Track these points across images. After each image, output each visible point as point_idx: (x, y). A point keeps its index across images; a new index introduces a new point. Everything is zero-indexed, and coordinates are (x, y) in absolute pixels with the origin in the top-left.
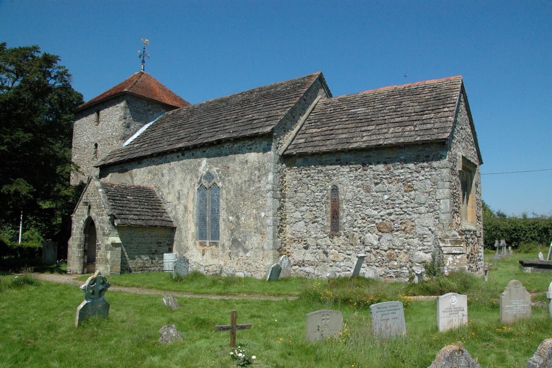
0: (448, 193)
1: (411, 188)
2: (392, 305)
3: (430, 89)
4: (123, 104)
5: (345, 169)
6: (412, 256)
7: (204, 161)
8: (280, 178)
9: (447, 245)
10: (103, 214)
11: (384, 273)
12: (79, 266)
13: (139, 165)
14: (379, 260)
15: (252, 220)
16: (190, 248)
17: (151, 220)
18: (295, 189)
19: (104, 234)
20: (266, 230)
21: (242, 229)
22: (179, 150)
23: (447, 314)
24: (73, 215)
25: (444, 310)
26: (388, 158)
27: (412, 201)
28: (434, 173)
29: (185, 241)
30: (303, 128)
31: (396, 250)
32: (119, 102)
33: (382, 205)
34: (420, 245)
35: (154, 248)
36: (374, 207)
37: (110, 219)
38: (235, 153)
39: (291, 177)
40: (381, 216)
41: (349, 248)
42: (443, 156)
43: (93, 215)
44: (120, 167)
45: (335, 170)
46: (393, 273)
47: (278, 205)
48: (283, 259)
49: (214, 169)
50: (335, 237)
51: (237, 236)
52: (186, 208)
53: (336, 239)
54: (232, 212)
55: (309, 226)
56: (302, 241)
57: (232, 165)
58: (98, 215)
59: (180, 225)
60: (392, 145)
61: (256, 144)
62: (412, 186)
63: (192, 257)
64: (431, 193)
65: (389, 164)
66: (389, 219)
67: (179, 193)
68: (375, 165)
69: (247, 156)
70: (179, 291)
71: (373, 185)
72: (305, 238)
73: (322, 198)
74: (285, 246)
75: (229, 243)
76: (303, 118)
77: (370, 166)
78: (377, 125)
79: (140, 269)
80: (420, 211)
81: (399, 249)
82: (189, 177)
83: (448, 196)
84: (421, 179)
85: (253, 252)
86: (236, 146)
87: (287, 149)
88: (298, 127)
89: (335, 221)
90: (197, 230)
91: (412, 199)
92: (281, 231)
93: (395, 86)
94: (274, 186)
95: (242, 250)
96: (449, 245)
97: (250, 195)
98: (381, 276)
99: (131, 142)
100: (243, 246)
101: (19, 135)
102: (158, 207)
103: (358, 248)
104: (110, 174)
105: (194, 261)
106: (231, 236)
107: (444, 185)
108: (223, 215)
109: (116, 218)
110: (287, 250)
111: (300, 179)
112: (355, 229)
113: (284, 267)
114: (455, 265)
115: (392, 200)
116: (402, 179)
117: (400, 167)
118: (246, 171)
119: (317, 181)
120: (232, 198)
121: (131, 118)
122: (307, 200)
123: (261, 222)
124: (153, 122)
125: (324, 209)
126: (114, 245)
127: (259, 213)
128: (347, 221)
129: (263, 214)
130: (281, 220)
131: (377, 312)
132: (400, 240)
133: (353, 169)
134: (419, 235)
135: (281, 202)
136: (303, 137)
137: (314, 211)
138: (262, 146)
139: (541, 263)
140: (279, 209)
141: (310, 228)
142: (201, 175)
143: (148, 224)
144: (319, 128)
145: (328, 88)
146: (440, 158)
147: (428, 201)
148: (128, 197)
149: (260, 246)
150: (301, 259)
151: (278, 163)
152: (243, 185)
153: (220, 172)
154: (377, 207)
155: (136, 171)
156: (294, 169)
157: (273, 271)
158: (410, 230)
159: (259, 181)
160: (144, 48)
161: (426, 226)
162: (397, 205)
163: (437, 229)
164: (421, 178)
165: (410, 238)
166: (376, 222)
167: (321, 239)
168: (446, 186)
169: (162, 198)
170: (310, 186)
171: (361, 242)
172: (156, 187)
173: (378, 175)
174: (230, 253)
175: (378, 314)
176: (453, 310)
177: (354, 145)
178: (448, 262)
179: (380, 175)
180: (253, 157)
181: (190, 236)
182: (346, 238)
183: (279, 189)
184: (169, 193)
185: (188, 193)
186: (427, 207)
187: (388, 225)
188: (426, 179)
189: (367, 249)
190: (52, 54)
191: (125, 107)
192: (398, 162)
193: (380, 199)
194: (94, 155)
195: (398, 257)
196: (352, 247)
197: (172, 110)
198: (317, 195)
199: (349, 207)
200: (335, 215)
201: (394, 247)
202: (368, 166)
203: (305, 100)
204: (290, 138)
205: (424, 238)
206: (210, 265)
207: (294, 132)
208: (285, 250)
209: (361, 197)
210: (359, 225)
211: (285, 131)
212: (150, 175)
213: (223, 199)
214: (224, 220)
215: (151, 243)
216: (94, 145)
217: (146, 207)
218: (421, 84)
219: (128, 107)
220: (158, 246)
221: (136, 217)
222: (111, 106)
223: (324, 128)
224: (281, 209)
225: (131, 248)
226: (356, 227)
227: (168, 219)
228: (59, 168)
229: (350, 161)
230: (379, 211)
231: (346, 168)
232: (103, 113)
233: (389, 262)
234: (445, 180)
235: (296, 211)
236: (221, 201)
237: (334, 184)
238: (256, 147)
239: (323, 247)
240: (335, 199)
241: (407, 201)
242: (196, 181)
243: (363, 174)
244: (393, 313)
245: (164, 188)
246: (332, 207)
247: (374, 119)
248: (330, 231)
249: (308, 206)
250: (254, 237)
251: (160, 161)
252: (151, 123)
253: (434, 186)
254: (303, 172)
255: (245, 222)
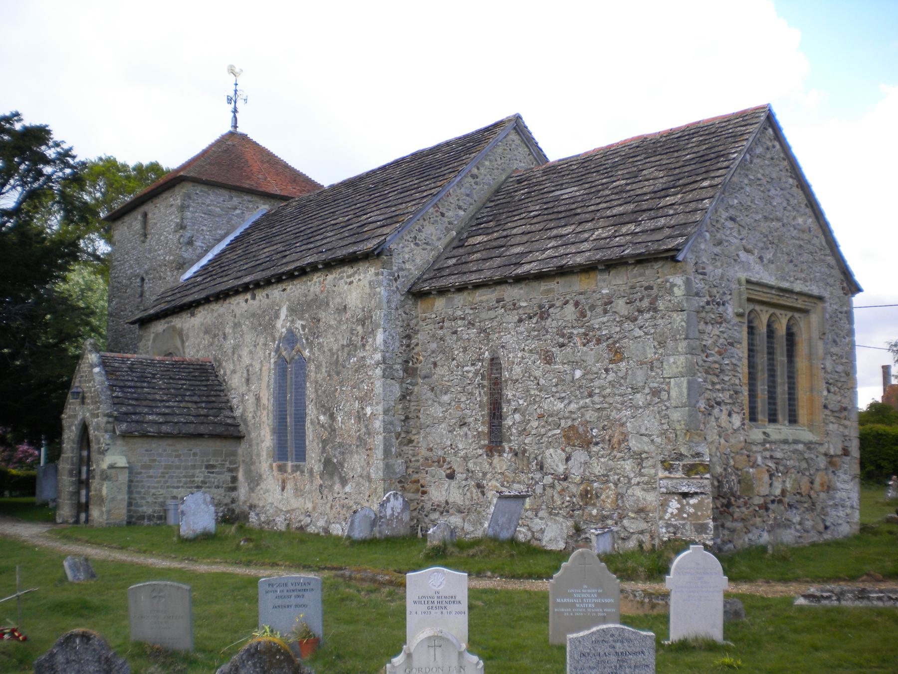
0: (684, 365)
9: (672, 476)
15: (353, 422)
20: (374, 441)
23: (424, 607)
25: (417, 599)
26: (581, 294)
27: (622, 381)
52: (258, 399)
53: (496, 459)
55: (455, 433)
59: (249, 433)
61: (359, 274)
63: (267, 494)
67: (248, 371)
82: (262, 340)
84: (637, 335)
90: (275, 441)
91: (622, 378)
96: (679, 474)
99: (195, 273)
102: (214, 399)
105: (270, 501)
107: (677, 348)
108: (311, 410)
113: (393, 515)
114: (684, 519)
120: (324, 379)
123: (366, 426)
128: (514, 424)
149: (365, 473)
159: (364, 345)
174: (321, 486)
175: (270, 595)
176: (436, 600)
177: (526, 268)
181: (264, 454)
185: (261, 370)
188: (646, 334)
194: (139, 300)
200: (495, 413)
212: (207, 337)
213: (311, 382)
214: (312, 423)
215: (194, 467)
220: (209, 472)
225: (151, 477)
242: (273, 346)
244: (298, 596)
245: (226, 361)
250: (355, 456)
255: (343, 426)
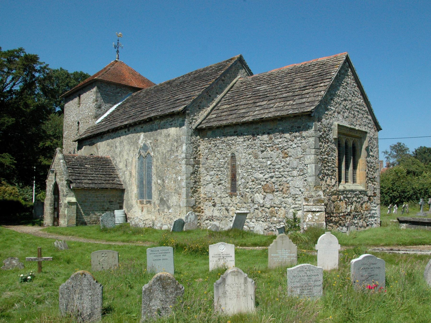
1: (286, 155)
2: (164, 249)
3: (319, 66)
4: (95, 89)
5: (240, 139)
6: (287, 213)
7: (142, 135)
8: (195, 148)
9: (309, 204)
10: (63, 179)
11: (267, 227)
12: (50, 220)
13: (102, 140)
14: (264, 216)
16: (134, 206)
17: (103, 183)
18: (206, 157)
19: (64, 196)
21: (166, 190)
22: (126, 126)
24: (47, 181)
25: (214, 256)
26: (270, 129)
27: (288, 166)
28: (304, 141)
29: (131, 200)
30: (219, 105)
31: (276, 208)
32: (92, 88)
33: (266, 169)
34: (293, 204)
35: (107, 206)
36: (260, 172)
37: (67, 184)
38: (162, 129)
39: (203, 147)
40: (266, 179)
41: (243, 206)
42: (310, 126)
43: (58, 180)
44: (90, 141)
45: (233, 140)
46: (274, 228)
47: (191, 169)
48: (189, 215)
49: (149, 141)
50: (234, 197)
51: (163, 196)
52: (131, 173)
54: (159, 176)
55: (216, 187)
56: (211, 200)
57: (159, 138)
58: (60, 180)
59: (127, 188)
60: (271, 118)
61: (175, 121)
62: (288, 153)
63: (135, 213)
64: (301, 159)
65: (271, 134)
66: (271, 181)
67: (126, 161)
68: (262, 136)
69: (169, 130)
70: (98, 239)
71: (260, 153)
72: (213, 197)
73: (225, 164)
74: (200, 203)
75: (158, 202)
76: (219, 97)
77: (258, 136)
78: (269, 100)
79: (94, 223)
80: (293, 175)
81: (278, 207)
82: (132, 149)
83: (314, 161)
84: (294, 147)
85: (173, 209)
86: (162, 122)
87: (201, 123)
88: (214, 104)
89: (234, 183)
90: (138, 191)
92: (195, 192)
93: (295, 65)
94: (187, 154)
95: (166, 207)
96: (312, 204)
97: (171, 162)
98: (266, 229)
100: (167, 204)
101: (4, 120)
102: (112, 173)
103: (249, 206)
104: (84, 147)
105: (136, 216)
106: (159, 196)
107: (311, 152)
108: (154, 178)
109: (71, 182)
110: (202, 207)
111: (210, 149)
112: (247, 190)
114: (314, 221)
115: (273, 165)
116: (280, 147)
117: (279, 136)
118: (169, 143)
119: (221, 150)
121: (102, 101)
122: (215, 166)
123: (178, 185)
124: (122, 102)
125: (226, 173)
126: (70, 203)
127: (177, 177)
128: (241, 184)
129: (179, 178)
130: (195, 182)
131: (150, 254)
132: (279, 199)
133: (246, 139)
134: (293, 195)
135: (195, 168)
136: (216, 113)
137: (219, 175)
138: (179, 122)
139: (414, 220)
140: (193, 173)
141: (216, 189)
142: (140, 146)
143: (100, 187)
144: (229, 105)
145: (248, 68)
146: (307, 128)
147: (299, 165)
148: (86, 166)
149: (178, 204)
150: (211, 215)
151: (191, 136)
152: (167, 154)
153: (152, 144)
154: (263, 171)
155: (100, 144)
156: (206, 140)
157: (176, 224)
158: (286, 191)
159: (177, 151)
160: (118, 40)
161: (297, 188)
162: (277, 170)
163: (305, 190)
164: (294, 146)
165: (286, 198)
166: (262, 184)
167: (224, 198)
168: (312, 153)
169: (116, 166)
170: (216, 154)
171: (251, 201)
172: (112, 157)
173: (264, 144)
174: (159, 209)
178: (308, 218)
179: (265, 144)
180: (173, 131)
181: (134, 196)
182: (241, 198)
183: (192, 157)
184: (120, 162)
185: (132, 161)
186: (298, 171)
187: (270, 186)
188: (298, 146)
189: (256, 207)
190: (32, 54)
191: (97, 92)
192: (277, 132)
193: (265, 164)
194: (77, 132)
195: (277, 213)
196: (245, 205)
197: (136, 92)
198: (221, 162)
199: (243, 171)
200: (234, 179)
201: (275, 205)
202: (256, 137)
203: (223, 80)
204: (205, 114)
205: (296, 198)
206: (147, 220)
207: (209, 109)
208: (200, 208)
209: (251, 162)
210: (250, 187)
211: (200, 108)
212: (108, 147)
213: (154, 166)
214: (155, 183)
215: (104, 202)
216: (77, 123)
217: (101, 173)
218: (314, 61)
219: (99, 92)
220: (110, 204)
221: (90, 182)
222: (87, 91)
223: (232, 104)
224: (195, 174)
226: (248, 188)
227: (118, 182)
228: (41, 144)
229: (244, 132)
230: (264, 174)
231: (241, 138)
232: (83, 96)
233: (271, 218)
234: (311, 147)
235: (207, 175)
236: (153, 167)
237: (233, 152)
238: (175, 123)
239: (225, 205)
240: (234, 165)
241: (284, 166)
242: (137, 151)
243: (252, 143)
244: (164, 255)
246: (232, 171)
247: (268, 95)
248: (230, 191)
249: (215, 171)
250: (174, 197)
251: (114, 136)
252: (120, 104)
253: (303, 152)
254: (212, 142)
